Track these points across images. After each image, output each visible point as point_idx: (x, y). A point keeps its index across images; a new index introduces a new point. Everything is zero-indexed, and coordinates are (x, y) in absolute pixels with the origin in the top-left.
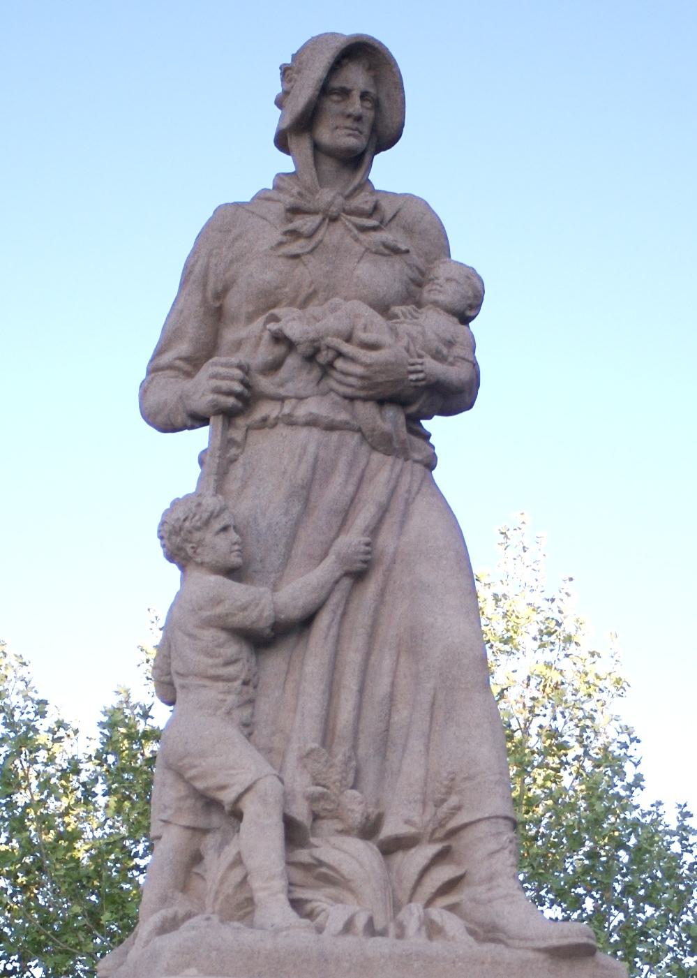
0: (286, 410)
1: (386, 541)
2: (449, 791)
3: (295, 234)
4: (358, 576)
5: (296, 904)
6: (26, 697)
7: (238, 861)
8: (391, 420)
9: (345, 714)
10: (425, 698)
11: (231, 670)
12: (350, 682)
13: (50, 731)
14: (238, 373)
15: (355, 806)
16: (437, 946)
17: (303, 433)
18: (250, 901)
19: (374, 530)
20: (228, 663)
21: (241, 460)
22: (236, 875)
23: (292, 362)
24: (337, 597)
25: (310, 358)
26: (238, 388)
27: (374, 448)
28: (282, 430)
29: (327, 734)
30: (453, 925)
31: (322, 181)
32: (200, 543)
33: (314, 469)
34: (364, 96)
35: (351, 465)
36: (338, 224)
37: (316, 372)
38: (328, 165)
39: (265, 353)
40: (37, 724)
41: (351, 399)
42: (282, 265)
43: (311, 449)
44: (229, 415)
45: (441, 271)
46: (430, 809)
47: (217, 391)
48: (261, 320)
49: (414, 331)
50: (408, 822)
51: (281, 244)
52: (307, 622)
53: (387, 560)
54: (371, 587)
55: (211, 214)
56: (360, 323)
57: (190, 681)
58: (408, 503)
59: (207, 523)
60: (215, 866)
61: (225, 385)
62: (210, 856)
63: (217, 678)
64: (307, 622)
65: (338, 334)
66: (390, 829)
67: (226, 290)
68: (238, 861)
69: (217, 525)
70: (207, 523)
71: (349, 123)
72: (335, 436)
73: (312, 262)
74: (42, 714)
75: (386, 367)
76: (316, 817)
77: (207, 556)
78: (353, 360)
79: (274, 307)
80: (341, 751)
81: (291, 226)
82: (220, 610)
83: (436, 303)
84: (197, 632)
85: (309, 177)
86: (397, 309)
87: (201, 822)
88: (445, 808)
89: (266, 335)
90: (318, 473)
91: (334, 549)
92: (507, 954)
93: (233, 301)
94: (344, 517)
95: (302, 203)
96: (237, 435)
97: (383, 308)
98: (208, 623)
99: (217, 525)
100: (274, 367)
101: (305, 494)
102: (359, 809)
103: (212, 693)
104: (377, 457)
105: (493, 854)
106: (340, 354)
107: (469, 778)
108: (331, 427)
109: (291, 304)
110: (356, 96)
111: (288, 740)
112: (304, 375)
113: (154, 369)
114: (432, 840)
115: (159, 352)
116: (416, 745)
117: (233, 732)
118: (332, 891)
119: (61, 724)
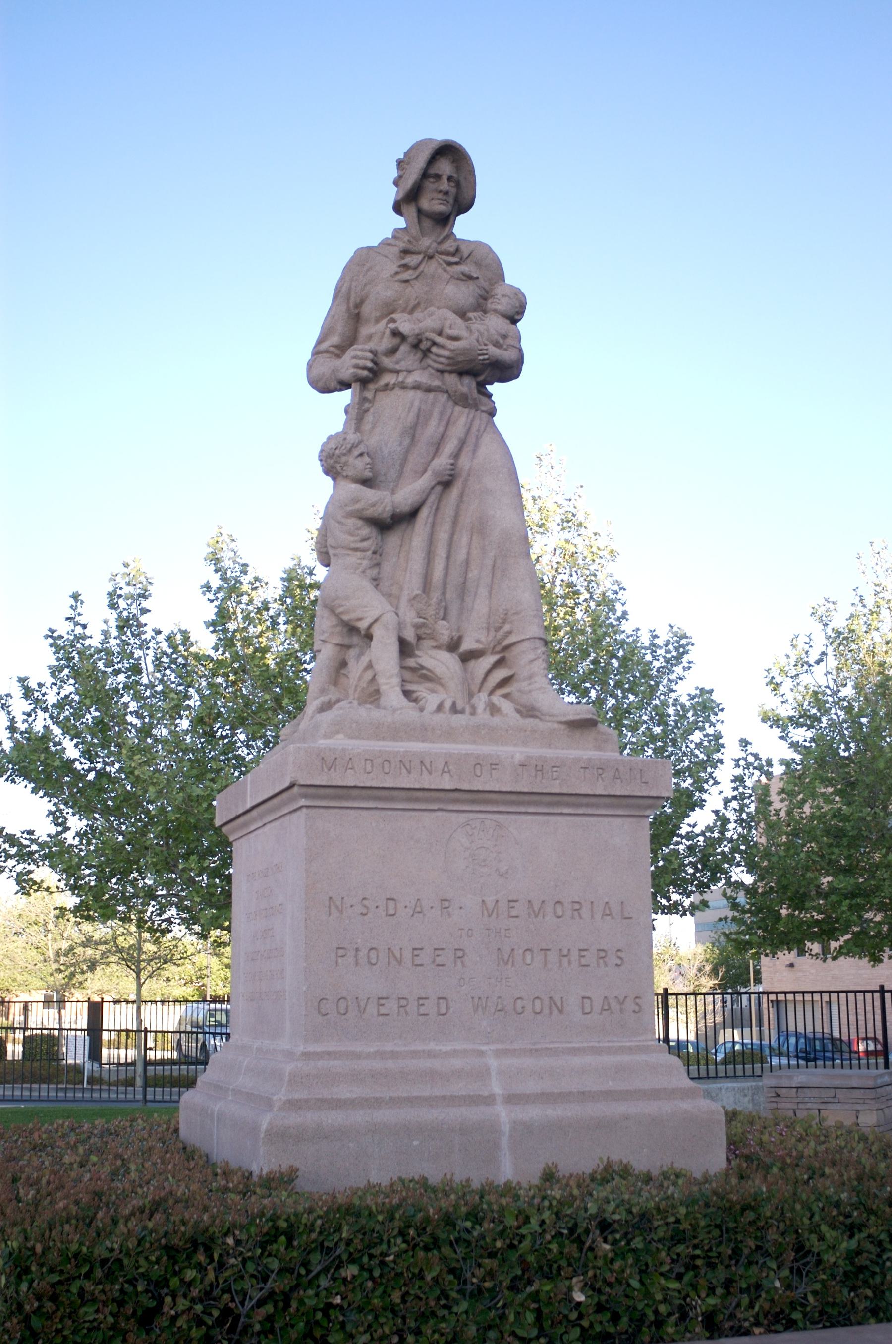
0: (400, 379)
1: (464, 462)
2: (504, 621)
3: (406, 267)
4: (446, 484)
5: (407, 693)
7: (370, 666)
8: (467, 385)
11: (365, 544)
12: (441, 552)
14: (370, 355)
15: (444, 631)
16: (496, 720)
17: (411, 393)
18: (377, 691)
19: (456, 455)
20: (363, 540)
21: (371, 411)
22: (369, 675)
23: (404, 348)
24: (433, 498)
25: (416, 346)
26: (370, 365)
27: (456, 403)
28: (398, 391)
30: (506, 706)
31: (423, 234)
32: (346, 464)
33: (418, 416)
34: (450, 179)
35: (442, 414)
36: (434, 261)
37: (419, 355)
38: (427, 223)
42: (398, 286)
43: (417, 403)
46: (492, 633)
47: (357, 367)
48: (385, 321)
50: (478, 641)
51: (397, 273)
52: (413, 514)
53: (464, 474)
54: (455, 492)
56: (448, 323)
57: (339, 551)
58: (478, 438)
59: (350, 451)
60: (355, 669)
61: (361, 363)
62: (352, 663)
64: (413, 514)
65: (433, 331)
66: (467, 645)
67: (362, 302)
68: (370, 666)
69: (356, 452)
70: (350, 451)
71: (440, 196)
72: (431, 395)
73: (417, 284)
75: (464, 351)
76: (419, 638)
77: (350, 472)
78: (442, 347)
79: (392, 313)
80: (435, 596)
81: (403, 262)
82: (358, 506)
83: (495, 311)
84: (343, 520)
85: (415, 230)
87: (346, 641)
88: (501, 632)
89: (388, 331)
90: (421, 420)
91: (430, 468)
94: (437, 447)
95: (410, 247)
96: (369, 394)
97: (462, 314)
98: (350, 514)
99: (356, 452)
100: (393, 351)
101: (412, 432)
103: (353, 559)
104: (458, 409)
106: (434, 343)
108: (429, 390)
112: (412, 357)
113: (316, 353)
114: (493, 653)
115: (319, 342)
116: (483, 592)
117: (367, 584)
119: (257, 579)
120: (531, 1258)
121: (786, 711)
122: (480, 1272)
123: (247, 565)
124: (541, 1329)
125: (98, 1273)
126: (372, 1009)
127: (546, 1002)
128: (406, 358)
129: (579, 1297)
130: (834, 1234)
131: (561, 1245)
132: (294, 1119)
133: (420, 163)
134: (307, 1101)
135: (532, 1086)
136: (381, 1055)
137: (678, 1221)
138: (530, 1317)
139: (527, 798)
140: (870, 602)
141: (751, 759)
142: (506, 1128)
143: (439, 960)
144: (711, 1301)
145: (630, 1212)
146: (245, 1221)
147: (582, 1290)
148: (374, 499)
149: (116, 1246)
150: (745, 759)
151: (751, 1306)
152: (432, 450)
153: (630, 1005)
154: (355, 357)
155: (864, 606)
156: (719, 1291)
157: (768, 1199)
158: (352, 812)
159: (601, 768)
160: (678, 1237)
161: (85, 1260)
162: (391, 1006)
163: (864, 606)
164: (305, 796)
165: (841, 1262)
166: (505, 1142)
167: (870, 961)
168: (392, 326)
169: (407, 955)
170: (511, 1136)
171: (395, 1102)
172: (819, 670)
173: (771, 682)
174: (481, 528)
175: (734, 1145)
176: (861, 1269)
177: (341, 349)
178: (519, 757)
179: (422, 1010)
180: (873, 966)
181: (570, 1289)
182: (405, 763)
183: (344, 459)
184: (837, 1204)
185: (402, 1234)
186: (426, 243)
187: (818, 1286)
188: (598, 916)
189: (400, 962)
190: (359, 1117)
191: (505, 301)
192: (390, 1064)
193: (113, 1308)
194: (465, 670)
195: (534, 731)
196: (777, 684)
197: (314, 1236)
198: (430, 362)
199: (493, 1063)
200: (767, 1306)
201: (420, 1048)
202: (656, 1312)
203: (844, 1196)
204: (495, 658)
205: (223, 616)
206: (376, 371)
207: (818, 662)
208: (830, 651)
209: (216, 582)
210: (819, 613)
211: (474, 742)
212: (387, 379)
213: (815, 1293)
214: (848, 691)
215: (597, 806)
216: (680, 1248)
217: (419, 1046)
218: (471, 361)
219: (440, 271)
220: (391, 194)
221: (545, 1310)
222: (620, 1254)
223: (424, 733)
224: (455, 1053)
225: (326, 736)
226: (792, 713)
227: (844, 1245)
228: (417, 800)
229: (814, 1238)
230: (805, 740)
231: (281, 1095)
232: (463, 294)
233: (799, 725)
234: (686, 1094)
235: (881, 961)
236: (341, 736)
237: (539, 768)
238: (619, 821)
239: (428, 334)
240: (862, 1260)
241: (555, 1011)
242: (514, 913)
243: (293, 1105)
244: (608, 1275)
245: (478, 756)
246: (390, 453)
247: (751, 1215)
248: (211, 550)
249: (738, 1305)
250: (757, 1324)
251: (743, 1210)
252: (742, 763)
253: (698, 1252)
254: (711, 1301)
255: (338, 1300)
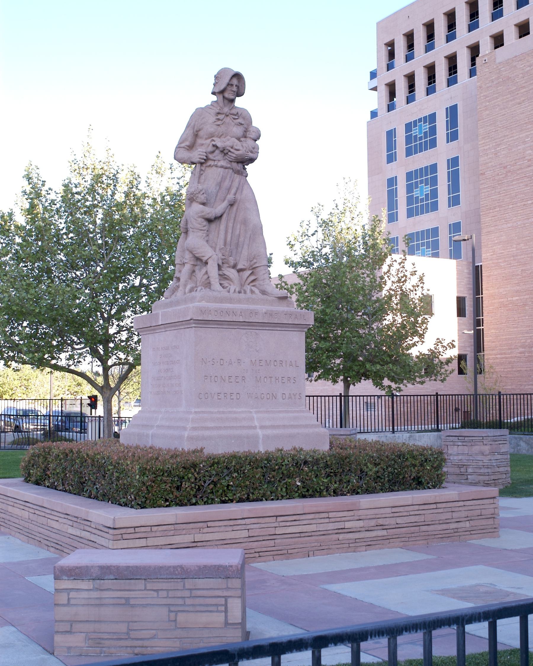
0: (216, 163)
1: (238, 196)
2: (254, 258)
3: (219, 119)
4: (232, 205)
5: (221, 284)
6: (38, 179)
7: (206, 273)
8: (239, 167)
9: (229, 239)
10: (248, 236)
11: (205, 228)
12: (230, 231)
13: (47, 191)
14: (205, 154)
15: (232, 261)
16: (254, 296)
17: (220, 169)
18: (210, 283)
19: (235, 194)
20: (204, 227)
21: (204, 174)
22: (206, 277)
23: (217, 152)
25: (222, 152)
26: (205, 158)
27: (235, 173)
28: (214, 168)
29: (225, 244)
31: (225, 106)
32: (198, 197)
33: (222, 178)
34: (236, 86)
35: (230, 177)
36: (228, 117)
37: (223, 154)
38: (226, 101)
39: (211, 149)
40: (42, 189)
41: (231, 162)
42: (215, 127)
43: (221, 173)
44: (202, 164)
45: (251, 129)
46: (249, 262)
47: (200, 158)
48: (210, 140)
49: (246, 145)
50: (244, 265)
52: (221, 216)
53: (238, 201)
54: (235, 208)
55: (194, 110)
56: (235, 144)
57: (194, 230)
58: (242, 187)
59: (199, 192)
61: (202, 157)
62: (197, 271)
63: (201, 230)
64: (221, 216)
65: (230, 147)
66: (240, 266)
67: (199, 130)
68: (206, 273)
69: (202, 193)
70: (199, 192)
71: (232, 93)
72: (227, 170)
73: (222, 126)
74: (43, 185)
75: (241, 155)
76: (223, 263)
77: (199, 200)
78: (233, 153)
79: (213, 137)
80: (228, 248)
81: (218, 117)
82: (203, 214)
83: (250, 138)
84: (197, 219)
85: (221, 104)
86: (242, 139)
87: (195, 264)
88: (253, 262)
89: (211, 145)
90: (223, 179)
91: (227, 199)
92: (269, 298)
93: (201, 133)
94: (229, 190)
95: (220, 112)
96: (203, 168)
97: (239, 139)
98: (200, 217)
99: (202, 193)
100: (213, 152)
101: (220, 185)
102: (232, 262)
103: (200, 233)
104: (236, 175)
105: (264, 274)
106: (230, 151)
107: (259, 256)
108: (226, 168)
109: (217, 137)
110: (234, 85)
111: (216, 245)
112: (220, 155)
113: (178, 147)
114: (249, 270)
115: (180, 143)
116: (246, 247)
117: (205, 243)
118: (228, 281)
119: (50, 189)
120: (285, 472)
121: (297, 259)
122: (271, 476)
123: (45, 181)
124: (287, 494)
125: (166, 474)
126: (216, 397)
127: (271, 395)
128: (218, 155)
129: (299, 484)
130: (371, 466)
131: (294, 468)
132: (195, 433)
133: (226, 80)
134: (198, 427)
135: (268, 423)
136: (219, 412)
137: (327, 462)
138: (284, 490)
139: (266, 324)
140: (341, 208)
141: (283, 284)
142: (261, 437)
143: (237, 380)
144: (336, 485)
145: (313, 458)
146: (206, 459)
147: (299, 482)
148: (208, 212)
149: (170, 467)
150: (281, 285)
151: (347, 487)
152: (227, 191)
153: (298, 397)
154: (199, 155)
155: (338, 209)
156: (338, 483)
157: (353, 455)
158: (209, 329)
159: (291, 314)
160: (327, 466)
161: (161, 471)
162: (222, 396)
163: (338, 209)
164: (195, 323)
165: (373, 475)
166: (260, 441)
167: (332, 382)
168: (214, 143)
169: (227, 378)
170: (263, 440)
171: (226, 428)
172: (313, 239)
173: (289, 244)
174: (245, 222)
175: (331, 443)
176: (378, 477)
177: (191, 147)
178: (264, 311)
179: (232, 397)
180: (334, 384)
181: (296, 482)
182: (227, 312)
183: (197, 195)
184: (372, 457)
185: (249, 464)
186: (226, 110)
187: (366, 482)
188: (288, 366)
189: (224, 381)
190: (215, 433)
191: (254, 134)
192: (223, 415)
193: (170, 485)
194: (239, 276)
195: (267, 300)
196: (292, 245)
197: (225, 464)
198: (227, 157)
199: (255, 416)
200: (351, 487)
201: (231, 410)
202: (320, 488)
203: (375, 454)
204: (251, 272)
205: (33, 206)
206: (207, 159)
207: (313, 235)
208: (320, 230)
209: (28, 188)
210: (314, 211)
211: (247, 304)
212: (210, 163)
213: (365, 484)
214: (327, 250)
215: (288, 327)
216: (327, 470)
217: (230, 410)
218: (242, 159)
219: (231, 121)
220: (211, 88)
221: (288, 488)
222: (311, 471)
223: (231, 300)
224: (242, 412)
225: (199, 302)
226: (299, 260)
227: (374, 469)
228: (231, 325)
229: (365, 467)
230: (305, 274)
231: (190, 425)
232: (238, 131)
233: (302, 266)
234: (316, 426)
235: (338, 382)
236: (204, 302)
237: (270, 314)
238: (295, 333)
239: (228, 148)
240: (379, 474)
241: (274, 398)
242: (261, 364)
243: (194, 429)
244: (307, 477)
245: (251, 310)
246: (211, 192)
247: (348, 460)
248: (26, 173)
249: (343, 487)
250: (349, 493)
251: (346, 458)
252: (279, 286)
253: (332, 471)
254: (336, 485)
255: (232, 483)
